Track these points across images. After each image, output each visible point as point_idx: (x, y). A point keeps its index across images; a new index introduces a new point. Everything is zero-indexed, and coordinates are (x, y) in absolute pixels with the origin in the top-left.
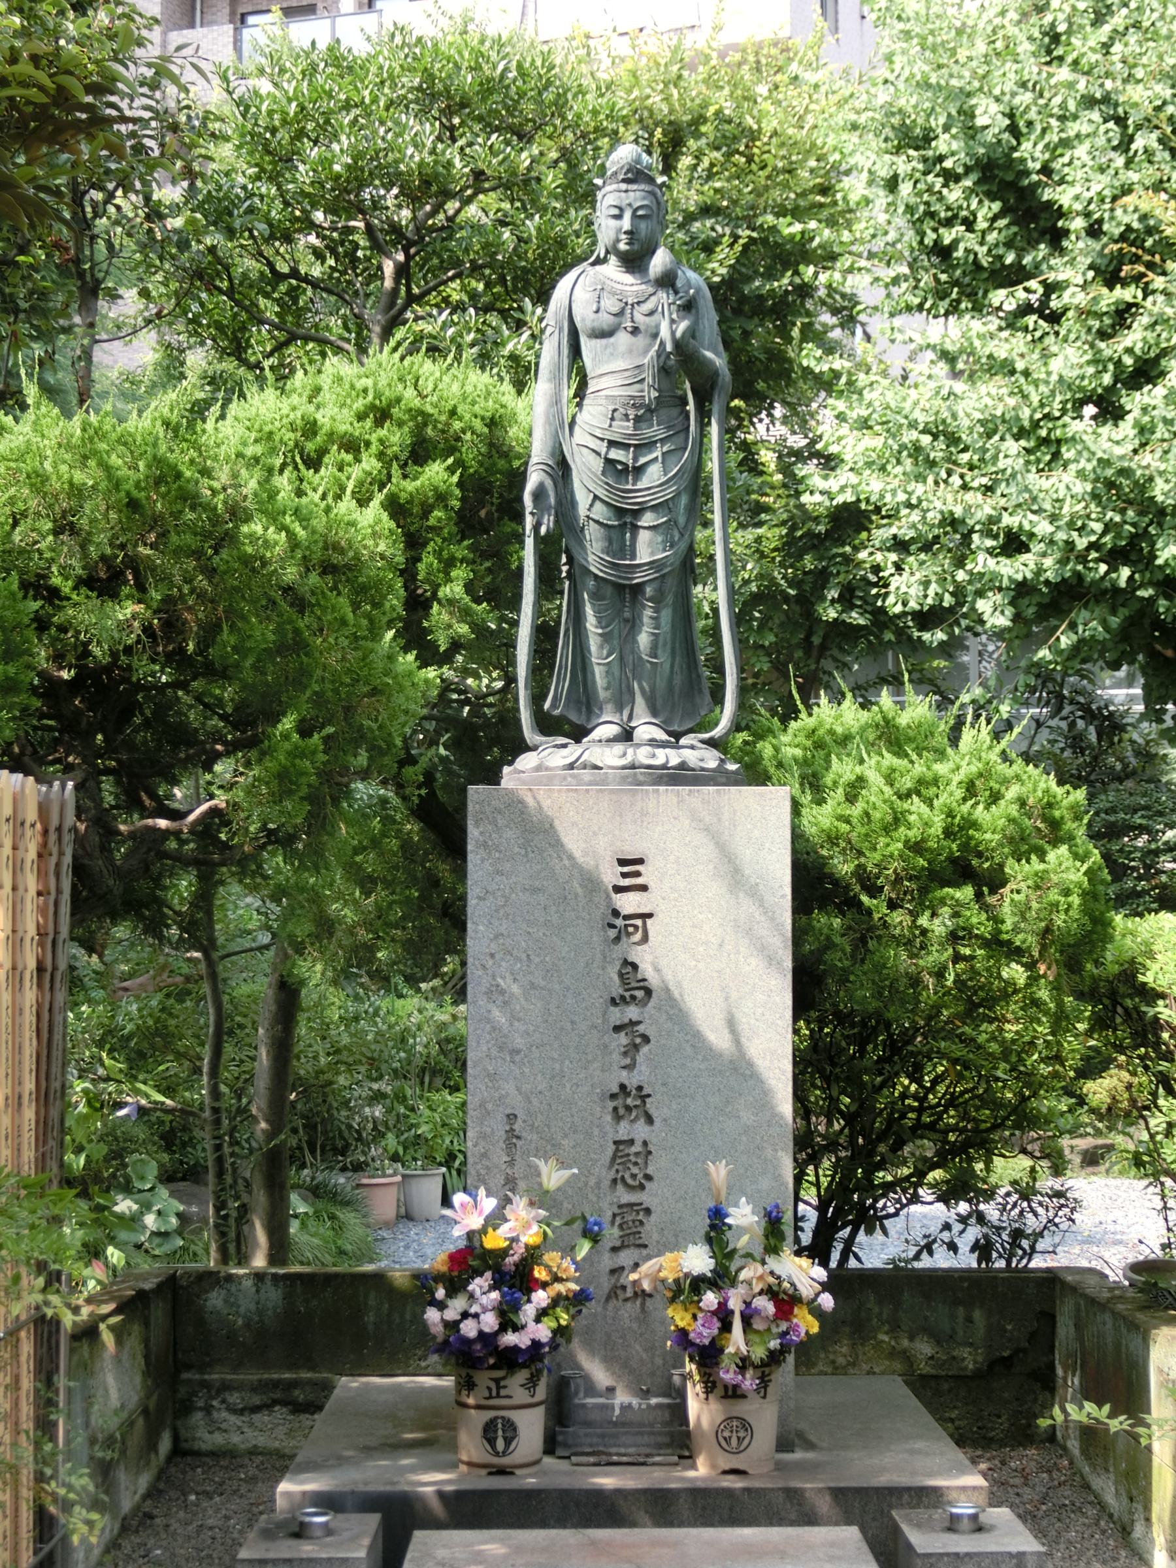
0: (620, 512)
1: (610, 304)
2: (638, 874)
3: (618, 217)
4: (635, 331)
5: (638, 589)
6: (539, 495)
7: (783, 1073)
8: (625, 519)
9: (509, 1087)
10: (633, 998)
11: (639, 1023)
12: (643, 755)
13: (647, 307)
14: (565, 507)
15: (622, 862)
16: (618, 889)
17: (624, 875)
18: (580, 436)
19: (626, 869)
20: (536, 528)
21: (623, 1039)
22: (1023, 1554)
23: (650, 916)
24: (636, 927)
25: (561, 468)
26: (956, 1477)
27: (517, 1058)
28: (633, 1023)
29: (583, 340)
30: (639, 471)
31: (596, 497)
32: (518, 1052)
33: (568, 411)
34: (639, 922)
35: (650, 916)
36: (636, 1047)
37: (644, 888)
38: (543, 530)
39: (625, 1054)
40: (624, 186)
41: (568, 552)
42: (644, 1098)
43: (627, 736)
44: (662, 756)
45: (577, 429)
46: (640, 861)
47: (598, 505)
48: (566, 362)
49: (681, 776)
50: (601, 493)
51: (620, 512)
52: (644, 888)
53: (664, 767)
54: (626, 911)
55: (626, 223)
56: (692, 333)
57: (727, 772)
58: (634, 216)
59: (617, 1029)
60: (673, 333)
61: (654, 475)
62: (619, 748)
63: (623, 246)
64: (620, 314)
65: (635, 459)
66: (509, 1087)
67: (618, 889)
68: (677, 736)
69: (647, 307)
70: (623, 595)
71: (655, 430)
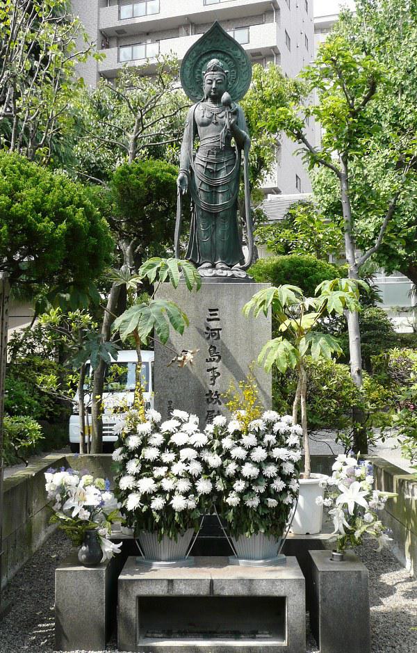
0: (211, 187)
1: (207, 114)
2: (216, 314)
3: (211, 84)
4: (216, 123)
5: (216, 215)
6: (182, 181)
7: (111, 66)
8: (213, 190)
9: (169, 391)
10: (214, 359)
11: (216, 368)
12: (218, 272)
13: (220, 115)
14: (191, 185)
15: (210, 310)
16: (209, 320)
17: (211, 315)
18: (197, 161)
19: (216, 317)
20: (181, 191)
21: (210, 374)
22: (360, 572)
23: (221, 329)
24: (215, 333)
25: (190, 174)
26: (138, 573)
27: (172, 381)
28: (214, 369)
29: (198, 127)
30: (218, 172)
31: (202, 182)
32: (173, 378)
33: (193, 152)
34: (217, 332)
35: (221, 329)
36: (216, 377)
37: (218, 319)
38: (183, 192)
39: (211, 380)
40: (212, 73)
41: (193, 202)
42: (218, 395)
43: (214, 266)
44: (225, 273)
45: (196, 159)
46: (217, 310)
47: (203, 185)
48: (192, 135)
49: (232, 279)
50: (203, 180)
51: (211, 187)
52: (218, 319)
53: (226, 276)
54: (213, 327)
55: (214, 86)
56: (237, 122)
57: (249, 279)
58: (216, 83)
59: (208, 370)
60: (230, 123)
61: (223, 175)
62: (210, 270)
63: (212, 94)
64: (211, 118)
65: (216, 168)
66: (169, 391)
67: (209, 320)
68: (231, 266)
69: (220, 115)
70: (211, 216)
71: (224, 159)
